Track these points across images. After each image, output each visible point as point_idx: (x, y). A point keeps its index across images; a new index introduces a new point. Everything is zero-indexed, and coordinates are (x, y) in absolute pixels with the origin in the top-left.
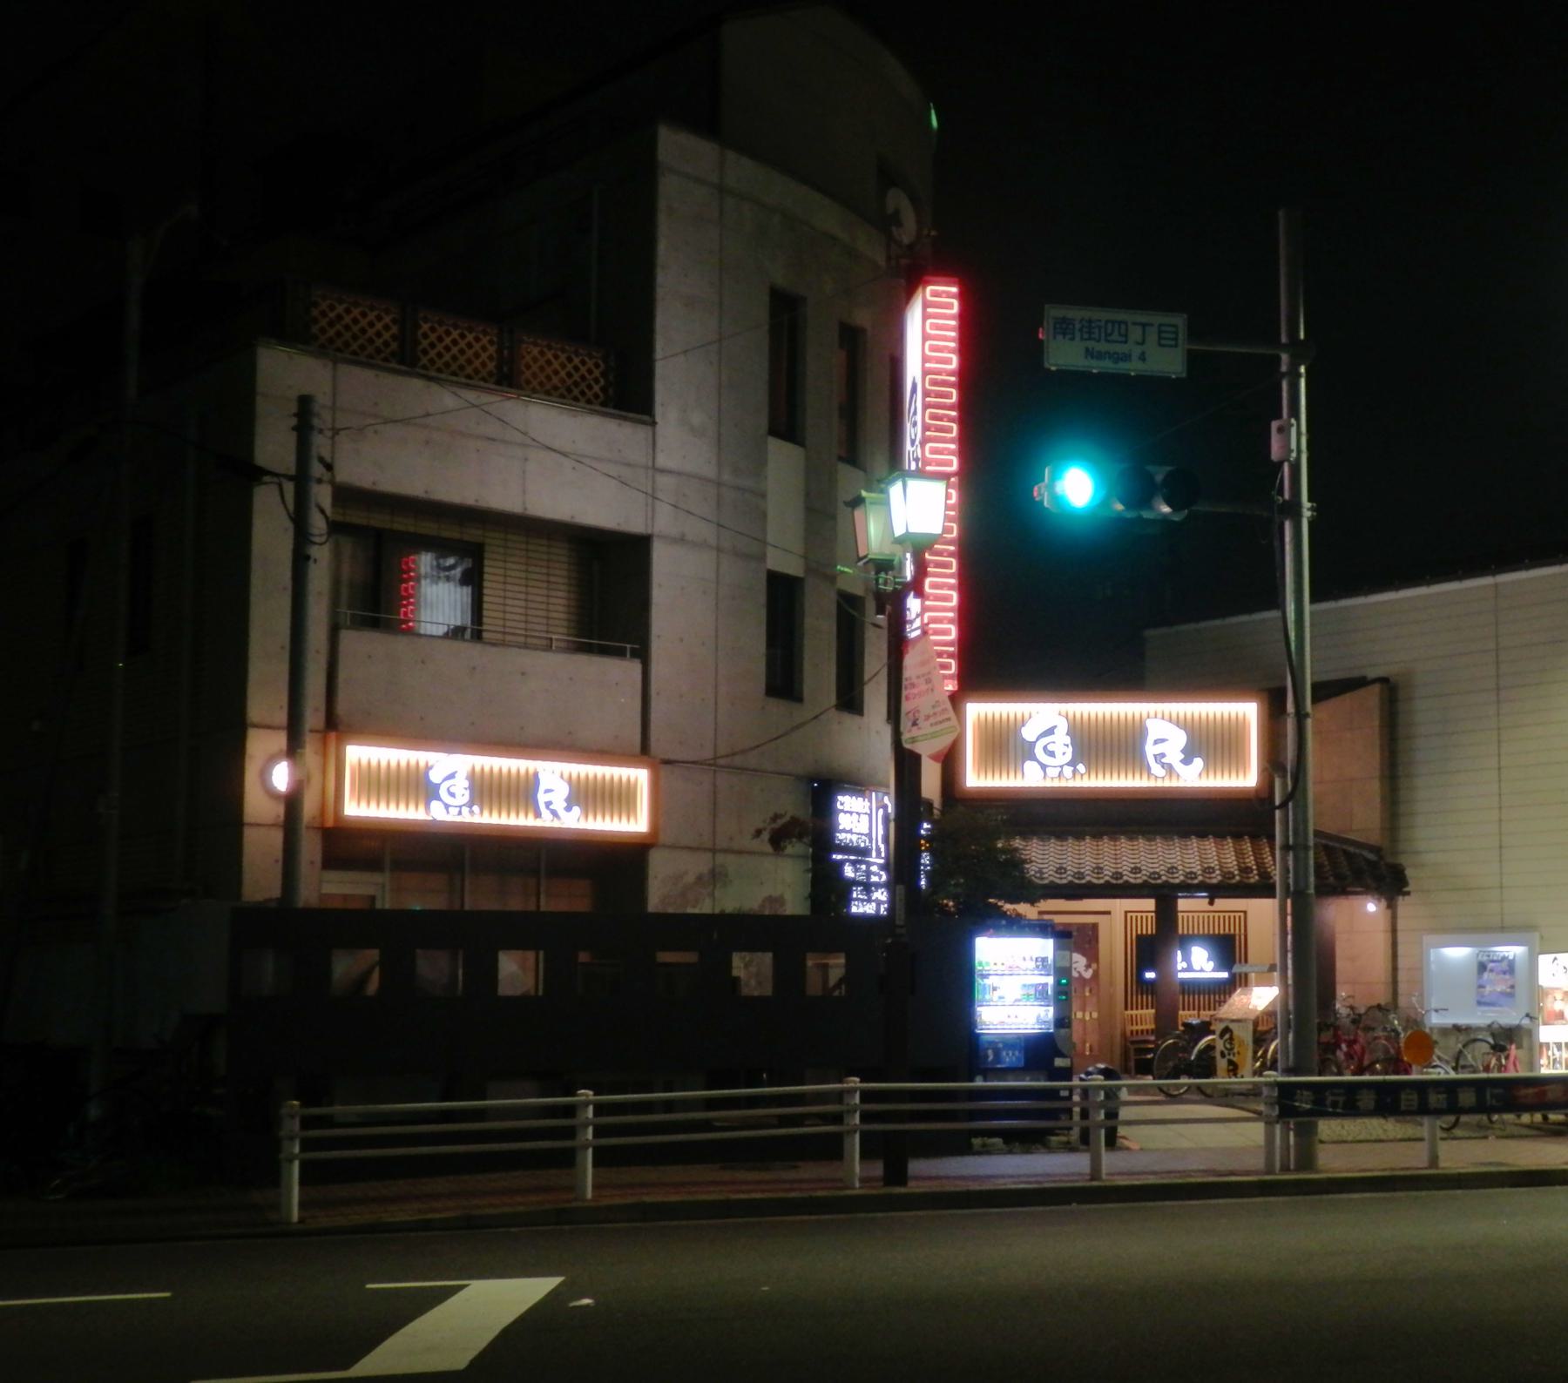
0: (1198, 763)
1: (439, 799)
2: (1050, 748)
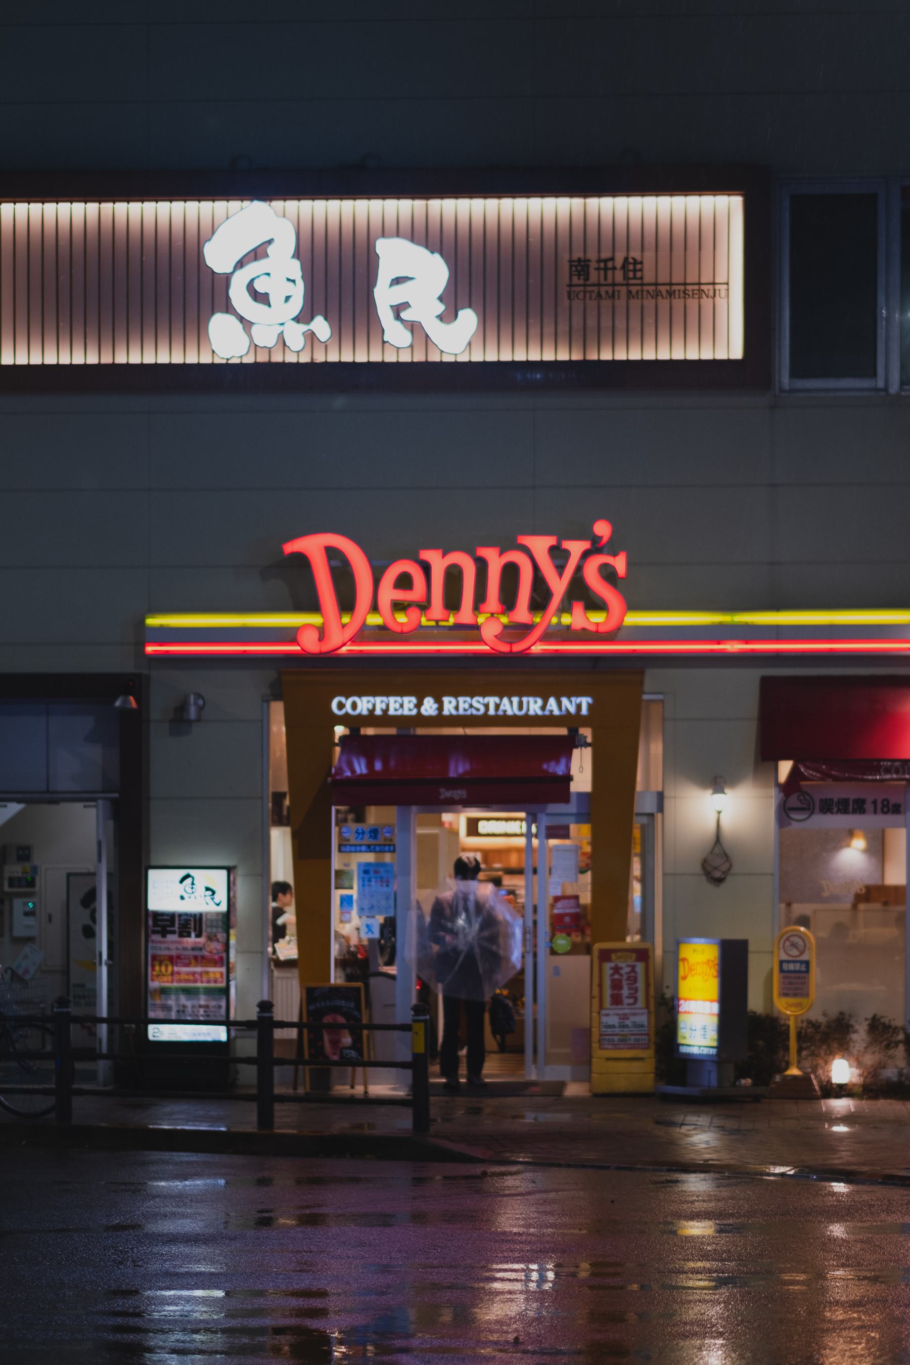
0: (468, 318)
1: (228, 308)
2: (260, 287)
